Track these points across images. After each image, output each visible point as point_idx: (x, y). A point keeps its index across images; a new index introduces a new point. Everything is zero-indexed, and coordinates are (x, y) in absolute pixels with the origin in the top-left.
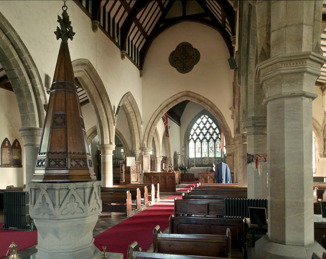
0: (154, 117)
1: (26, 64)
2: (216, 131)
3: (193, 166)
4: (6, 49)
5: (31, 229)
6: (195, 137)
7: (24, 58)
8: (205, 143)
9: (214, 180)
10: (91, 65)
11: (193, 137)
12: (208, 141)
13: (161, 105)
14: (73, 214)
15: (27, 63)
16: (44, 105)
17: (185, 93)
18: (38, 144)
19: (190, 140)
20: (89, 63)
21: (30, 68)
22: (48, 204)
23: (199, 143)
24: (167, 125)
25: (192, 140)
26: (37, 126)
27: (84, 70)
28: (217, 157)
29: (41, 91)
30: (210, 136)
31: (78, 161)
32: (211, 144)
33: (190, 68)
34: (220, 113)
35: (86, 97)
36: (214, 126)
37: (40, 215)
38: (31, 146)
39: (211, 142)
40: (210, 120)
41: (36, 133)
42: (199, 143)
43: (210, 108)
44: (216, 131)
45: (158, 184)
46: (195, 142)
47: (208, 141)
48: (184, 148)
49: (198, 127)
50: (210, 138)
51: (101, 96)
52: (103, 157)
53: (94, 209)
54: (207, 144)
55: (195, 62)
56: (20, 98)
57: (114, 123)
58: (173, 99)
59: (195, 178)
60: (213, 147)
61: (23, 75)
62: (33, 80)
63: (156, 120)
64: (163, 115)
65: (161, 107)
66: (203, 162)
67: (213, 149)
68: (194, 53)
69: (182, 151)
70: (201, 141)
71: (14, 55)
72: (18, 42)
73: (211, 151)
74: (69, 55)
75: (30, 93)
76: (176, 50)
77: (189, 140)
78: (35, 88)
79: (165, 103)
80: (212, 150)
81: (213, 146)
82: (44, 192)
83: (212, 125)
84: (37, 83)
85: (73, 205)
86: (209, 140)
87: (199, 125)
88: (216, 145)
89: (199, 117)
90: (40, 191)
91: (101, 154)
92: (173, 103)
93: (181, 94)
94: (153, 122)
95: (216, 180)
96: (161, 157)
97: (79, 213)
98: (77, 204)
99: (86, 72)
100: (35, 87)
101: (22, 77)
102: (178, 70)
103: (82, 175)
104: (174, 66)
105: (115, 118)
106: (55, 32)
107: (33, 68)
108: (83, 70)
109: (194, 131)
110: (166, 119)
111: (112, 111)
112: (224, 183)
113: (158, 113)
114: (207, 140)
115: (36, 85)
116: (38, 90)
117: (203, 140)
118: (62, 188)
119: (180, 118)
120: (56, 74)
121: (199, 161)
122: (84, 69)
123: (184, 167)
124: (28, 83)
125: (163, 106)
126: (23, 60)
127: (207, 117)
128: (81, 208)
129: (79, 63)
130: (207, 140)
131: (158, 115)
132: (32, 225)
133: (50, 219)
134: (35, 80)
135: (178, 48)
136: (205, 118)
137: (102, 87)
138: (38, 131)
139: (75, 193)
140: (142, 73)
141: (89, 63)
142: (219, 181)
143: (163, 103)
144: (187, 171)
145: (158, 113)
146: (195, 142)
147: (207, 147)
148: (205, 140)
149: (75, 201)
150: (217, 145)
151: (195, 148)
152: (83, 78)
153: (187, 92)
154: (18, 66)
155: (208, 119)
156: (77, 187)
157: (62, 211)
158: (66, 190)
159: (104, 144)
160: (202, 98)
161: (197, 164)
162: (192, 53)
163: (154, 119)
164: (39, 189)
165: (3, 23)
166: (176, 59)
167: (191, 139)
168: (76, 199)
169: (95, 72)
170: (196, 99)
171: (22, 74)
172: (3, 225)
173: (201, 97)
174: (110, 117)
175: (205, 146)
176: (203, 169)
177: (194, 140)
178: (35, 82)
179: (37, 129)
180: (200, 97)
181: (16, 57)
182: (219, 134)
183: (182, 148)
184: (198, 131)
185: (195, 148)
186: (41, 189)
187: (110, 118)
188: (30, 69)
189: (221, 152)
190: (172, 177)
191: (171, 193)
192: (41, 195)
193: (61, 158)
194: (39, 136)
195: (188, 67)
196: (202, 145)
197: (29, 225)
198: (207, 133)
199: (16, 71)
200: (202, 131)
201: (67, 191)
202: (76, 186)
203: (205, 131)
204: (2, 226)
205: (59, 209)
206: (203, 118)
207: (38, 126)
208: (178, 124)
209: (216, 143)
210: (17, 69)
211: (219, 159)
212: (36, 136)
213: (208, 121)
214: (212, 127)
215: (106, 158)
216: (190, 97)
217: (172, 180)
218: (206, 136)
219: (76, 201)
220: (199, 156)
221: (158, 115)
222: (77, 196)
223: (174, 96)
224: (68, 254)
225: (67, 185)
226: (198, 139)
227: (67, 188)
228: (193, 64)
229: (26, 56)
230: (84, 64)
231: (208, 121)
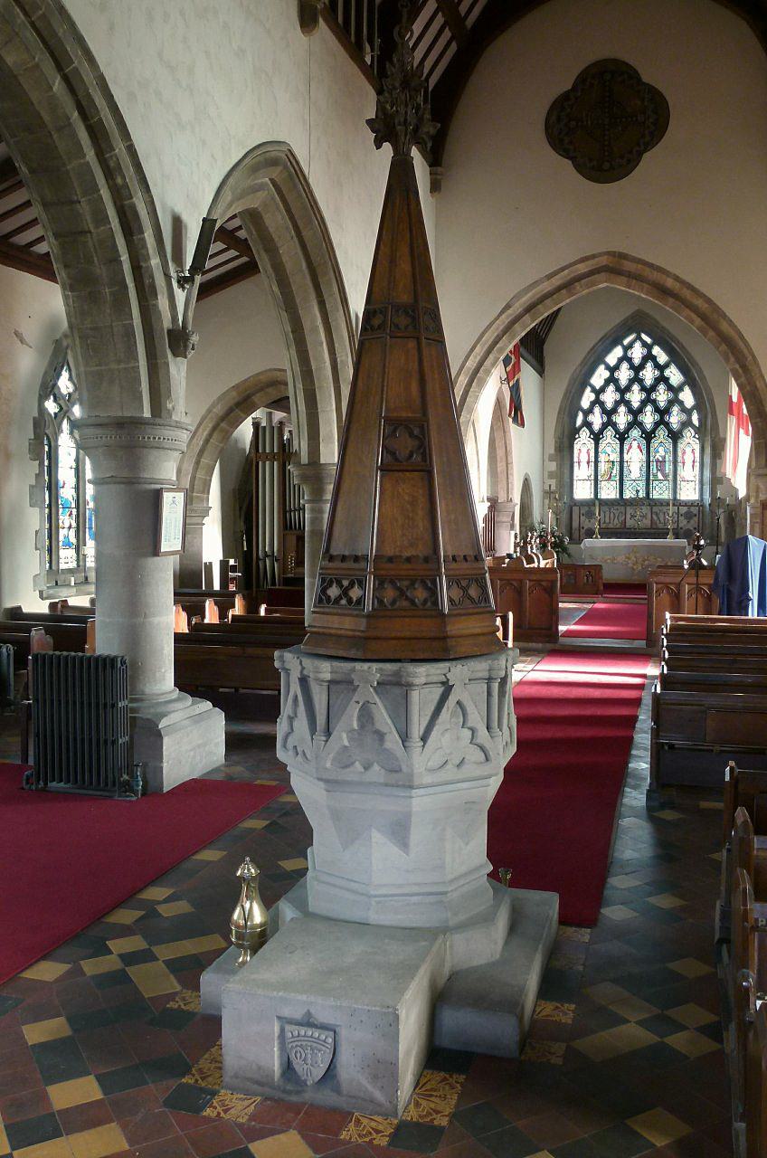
0: (480, 351)
1: (119, 181)
2: (682, 396)
3: (590, 534)
4: (60, 129)
5: (136, 793)
6: (597, 419)
7: (115, 159)
8: (635, 444)
9: (709, 598)
11: (590, 418)
12: (648, 436)
13: (508, 307)
15: (124, 177)
16: (169, 331)
17: (604, 261)
18: (146, 476)
19: (577, 431)
20: (289, 155)
21: (131, 194)
22: (381, 736)
23: (611, 441)
24: (516, 379)
25: (584, 433)
27: (269, 182)
28: (683, 501)
30: (657, 417)
31: (464, 583)
32: (661, 451)
33: (629, 161)
34: (741, 343)
35: (27, 204)
36: (675, 376)
37: (348, 770)
38: (122, 486)
39: (661, 439)
40: (656, 350)
41: (149, 438)
42: (611, 441)
43: (702, 319)
44: (682, 396)
45: (511, 615)
46: (597, 437)
47: (648, 436)
48: (555, 463)
49: (612, 380)
50: (657, 425)
51: (320, 280)
52: (312, 510)
53: (509, 744)
54: (644, 448)
55: (647, 139)
56: (86, 307)
58: (557, 281)
59: (604, 581)
60: (667, 459)
61: (106, 220)
62: (136, 242)
63: (488, 363)
64: (509, 345)
65: (509, 311)
66: (628, 516)
67: (669, 468)
68: (646, 103)
69: (546, 475)
70: (622, 437)
71: (84, 147)
72: (100, 102)
73: (659, 474)
74: (413, 206)
75: (126, 287)
76: (574, 88)
77: (573, 433)
78: (143, 271)
79: (526, 299)
80: (662, 471)
81: (669, 458)
82: (367, 693)
83: (667, 373)
84: (151, 251)
86: (653, 431)
87: (613, 370)
88: (680, 454)
89: (617, 341)
90: (355, 690)
91: (306, 498)
92: (555, 296)
93: (590, 263)
94: (477, 370)
95: (717, 602)
96: (483, 501)
98: (469, 733)
100: (142, 266)
101: (102, 228)
102: (578, 167)
103: (479, 635)
104: (566, 154)
106: (369, 122)
108: (267, 184)
109: (593, 397)
110: (513, 357)
112: (753, 615)
113: (496, 334)
114: (644, 431)
115: (147, 258)
116: (152, 277)
117: (628, 430)
119: (543, 342)
120: (377, 273)
121: (612, 515)
123: (558, 537)
125: (517, 308)
126: (112, 164)
127: (649, 340)
128: (482, 748)
129: (261, 159)
130: (644, 431)
131: (495, 342)
132: (139, 779)
133: (386, 785)
135: (583, 79)
136: (638, 344)
138: (149, 429)
140: (439, 177)
141: (289, 155)
142: (734, 605)
143: (517, 297)
144: (569, 555)
145: (498, 335)
146: (597, 437)
147: (644, 458)
148: (635, 433)
149: (464, 722)
150: (684, 453)
151: (596, 462)
152: (263, 215)
153: (614, 256)
154: (96, 189)
155: (649, 347)
158: (440, 685)
159: (322, 461)
160: (670, 283)
161: (603, 526)
162: (639, 103)
163: (479, 358)
164: (351, 682)
165: (60, 33)
166: (573, 124)
167: (581, 427)
169: (304, 189)
170: (646, 286)
171: (101, 218)
172: (27, 776)
173: (668, 276)
174: (344, 358)
175: (635, 457)
176: (632, 549)
177: (592, 432)
178: (144, 246)
179: (145, 424)
180: (664, 277)
181: (90, 155)
182: (693, 408)
183: (547, 460)
184: (610, 397)
185: (596, 462)
186: (356, 683)
188: (132, 198)
189: (697, 482)
190: (544, 583)
191: (540, 645)
192: (358, 702)
194: (152, 448)
195: (622, 157)
196: (625, 451)
197: (125, 777)
198: (644, 403)
199: (84, 208)
200: (627, 396)
201: (440, 690)
203: (635, 397)
204: (25, 777)
206: (630, 346)
207: (147, 414)
208: (535, 363)
209: (681, 446)
210: (90, 200)
211: (692, 509)
212: (144, 447)
213: (649, 357)
214: (666, 380)
216: (623, 275)
217: (547, 596)
218: (640, 418)
219: (469, 724)
220: (609, 492)
221: (495, 342)
223: (563, 269)
224: (432, 899)
225: (444, 672)
226: (610, 427)
227: (445, 680)
228: (638, 145)
229: (120, 148)
230: (274, 162)
231: (649, 357)
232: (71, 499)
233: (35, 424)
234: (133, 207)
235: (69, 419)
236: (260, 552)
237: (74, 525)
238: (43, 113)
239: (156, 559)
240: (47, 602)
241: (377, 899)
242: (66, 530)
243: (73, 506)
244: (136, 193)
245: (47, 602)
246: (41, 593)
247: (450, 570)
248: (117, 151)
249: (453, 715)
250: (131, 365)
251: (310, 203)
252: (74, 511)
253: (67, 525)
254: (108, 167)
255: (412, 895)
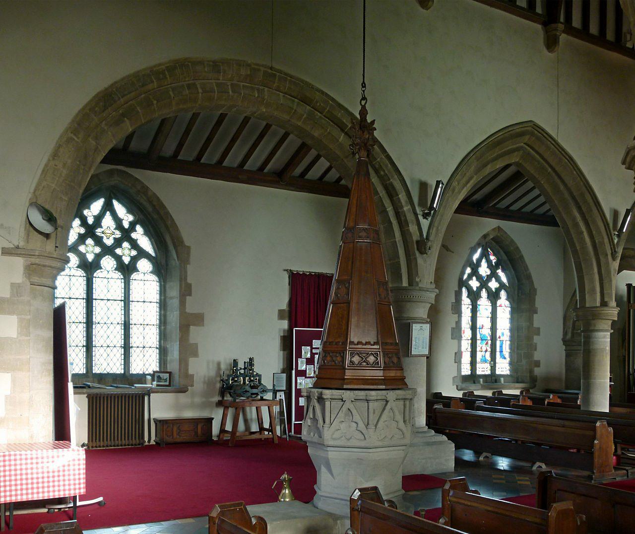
1: (382, 173)
7: (378, 164)
10: (540, 131)
14: (348, 440)
15: (384, 171)
26: (403, 283)
29: (410, 217)
57: (612, 254)
75: (391, 223)
85: (350, 426)
97: (358, 439)
98: (355, 425)
99: (531, 148)
105: (616, 241)
107: (396, 176)
108: (522, 147)
111: (608, 224)
115: (402, 207)
116: (405, 216)
118: (333, 397)
122: (524, 143)
124: (386, 205)
134: (399, 198)
137: (575, 172)
139: (351, 407)
156: (357, 398)
157: (333, 434)
165: (339, 115)
168: (354, 417)
187: (603, 243)
188: (389, 180)
193: (370, 351)
202: (355, 396)
205: (328, 430)
207: (405, 283)
215: (591, 340)
222: (354, 412)
232: (487, 335)
233: (455, 293)
234: (392, 185)
235: (486, 289)
236: (631, 369)
237: (489, 349)
238: (337, 152)
239: (407, 359)
240: (462, 392)
241: (324, 498)
242: (483, 353)
243: (489, 338)
244: (393, 177)
245: (462, 392)
246: (457, 386)
247: (385, 349)
248: (378, 159)
249: (346, 415)
250: (397, 261)
251: (558, 150)
252: (490, 342)
253: (484, 349)
254: (375, 167)
255: (336, 498)
